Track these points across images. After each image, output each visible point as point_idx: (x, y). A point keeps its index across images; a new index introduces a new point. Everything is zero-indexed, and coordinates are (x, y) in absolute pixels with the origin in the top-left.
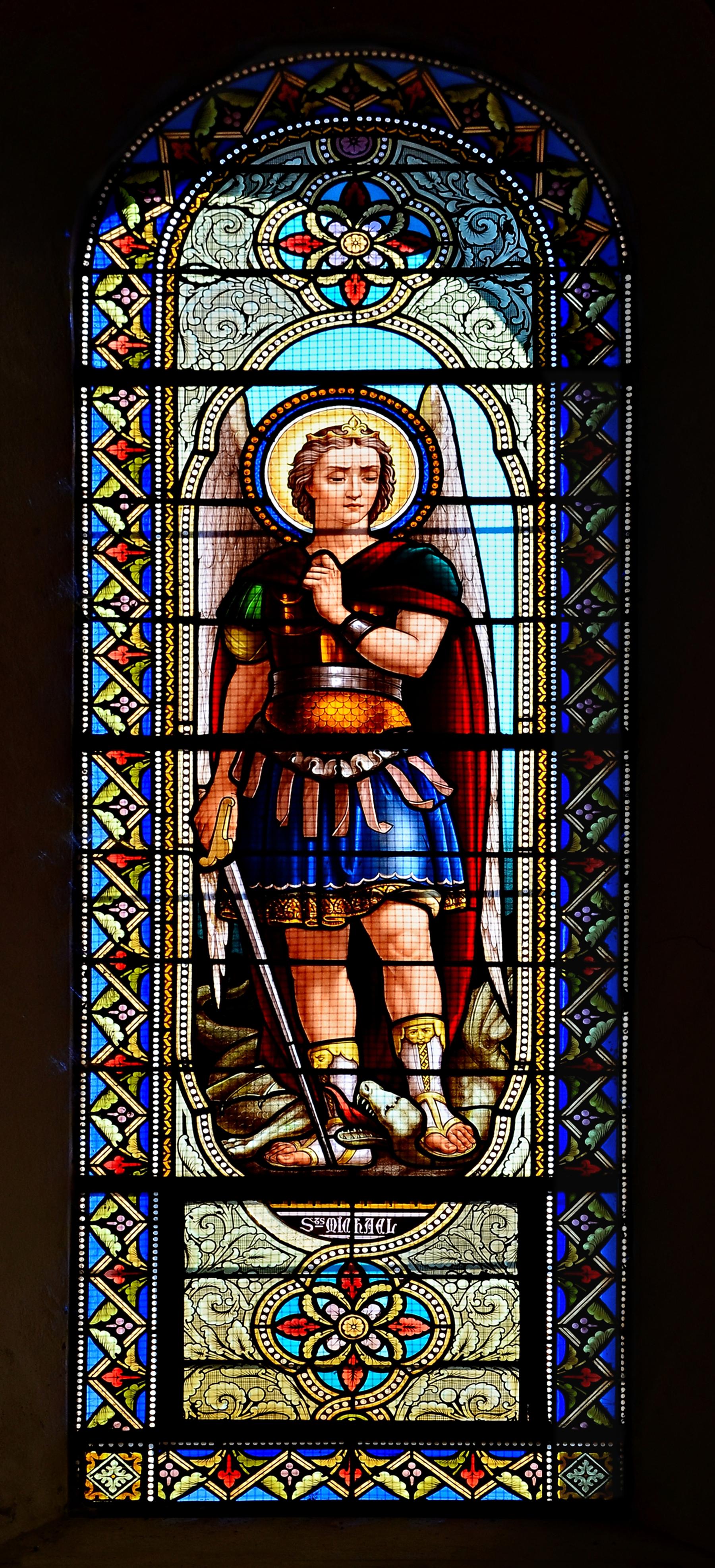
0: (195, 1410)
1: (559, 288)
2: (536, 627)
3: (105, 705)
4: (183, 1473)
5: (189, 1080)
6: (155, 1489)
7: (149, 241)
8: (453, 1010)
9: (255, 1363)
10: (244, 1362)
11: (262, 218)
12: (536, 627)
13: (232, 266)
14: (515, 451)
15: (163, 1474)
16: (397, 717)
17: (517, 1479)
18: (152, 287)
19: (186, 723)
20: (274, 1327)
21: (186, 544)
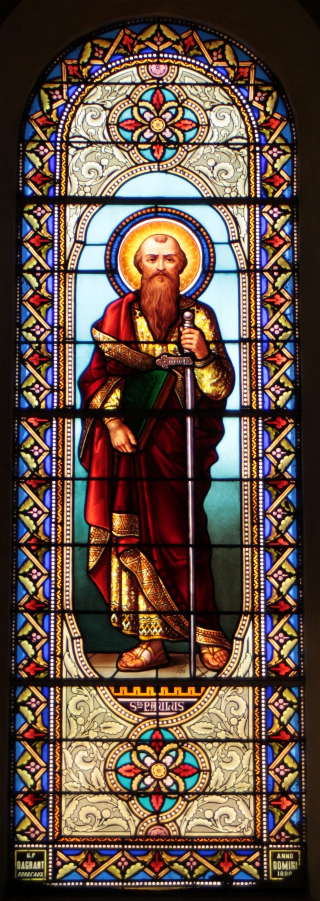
1: (261, 152)
11: (111, 110)
13: (96, 138)
14: (238, 241)
18: (55, 147)
21: (68, 485)
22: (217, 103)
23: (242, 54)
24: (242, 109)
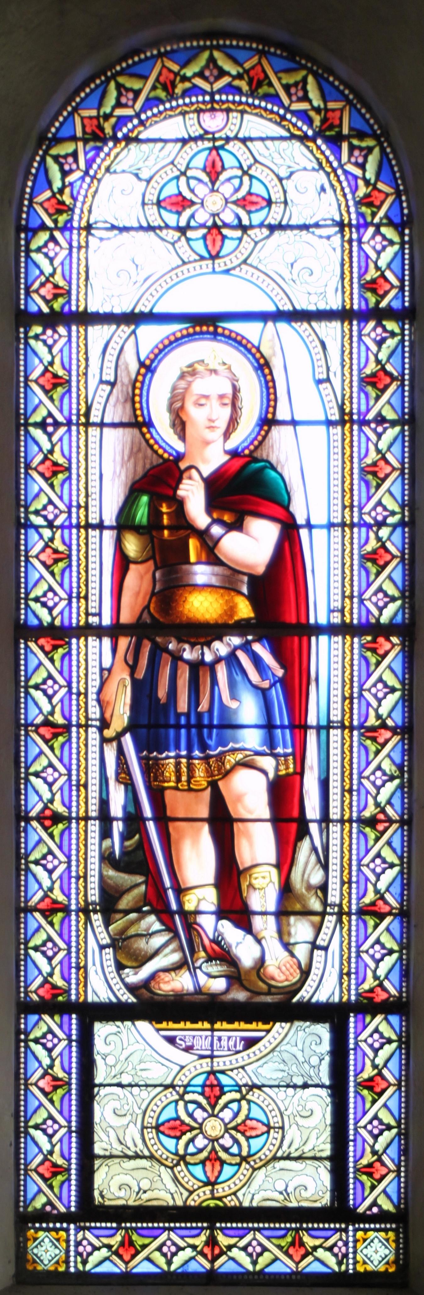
0: (102, 1197)
1: (360, 242)
2: (343, 531)
3: (37, 600)
4: (95, 1249)
5: (97, 919)
6: (76, 1262)
7: (67, 203)
8: (285, 861)
9: (144, 1157)
10: (137, 1156)
12: (343, 531)
14: (328, 380)
15: (81, 1249)
16: (244, 610)
17: (328, 1254)
19: (94, 615)
20: (157, 1128)
22: (296, 167)
23: (333, 90)
24: (332, 175)
